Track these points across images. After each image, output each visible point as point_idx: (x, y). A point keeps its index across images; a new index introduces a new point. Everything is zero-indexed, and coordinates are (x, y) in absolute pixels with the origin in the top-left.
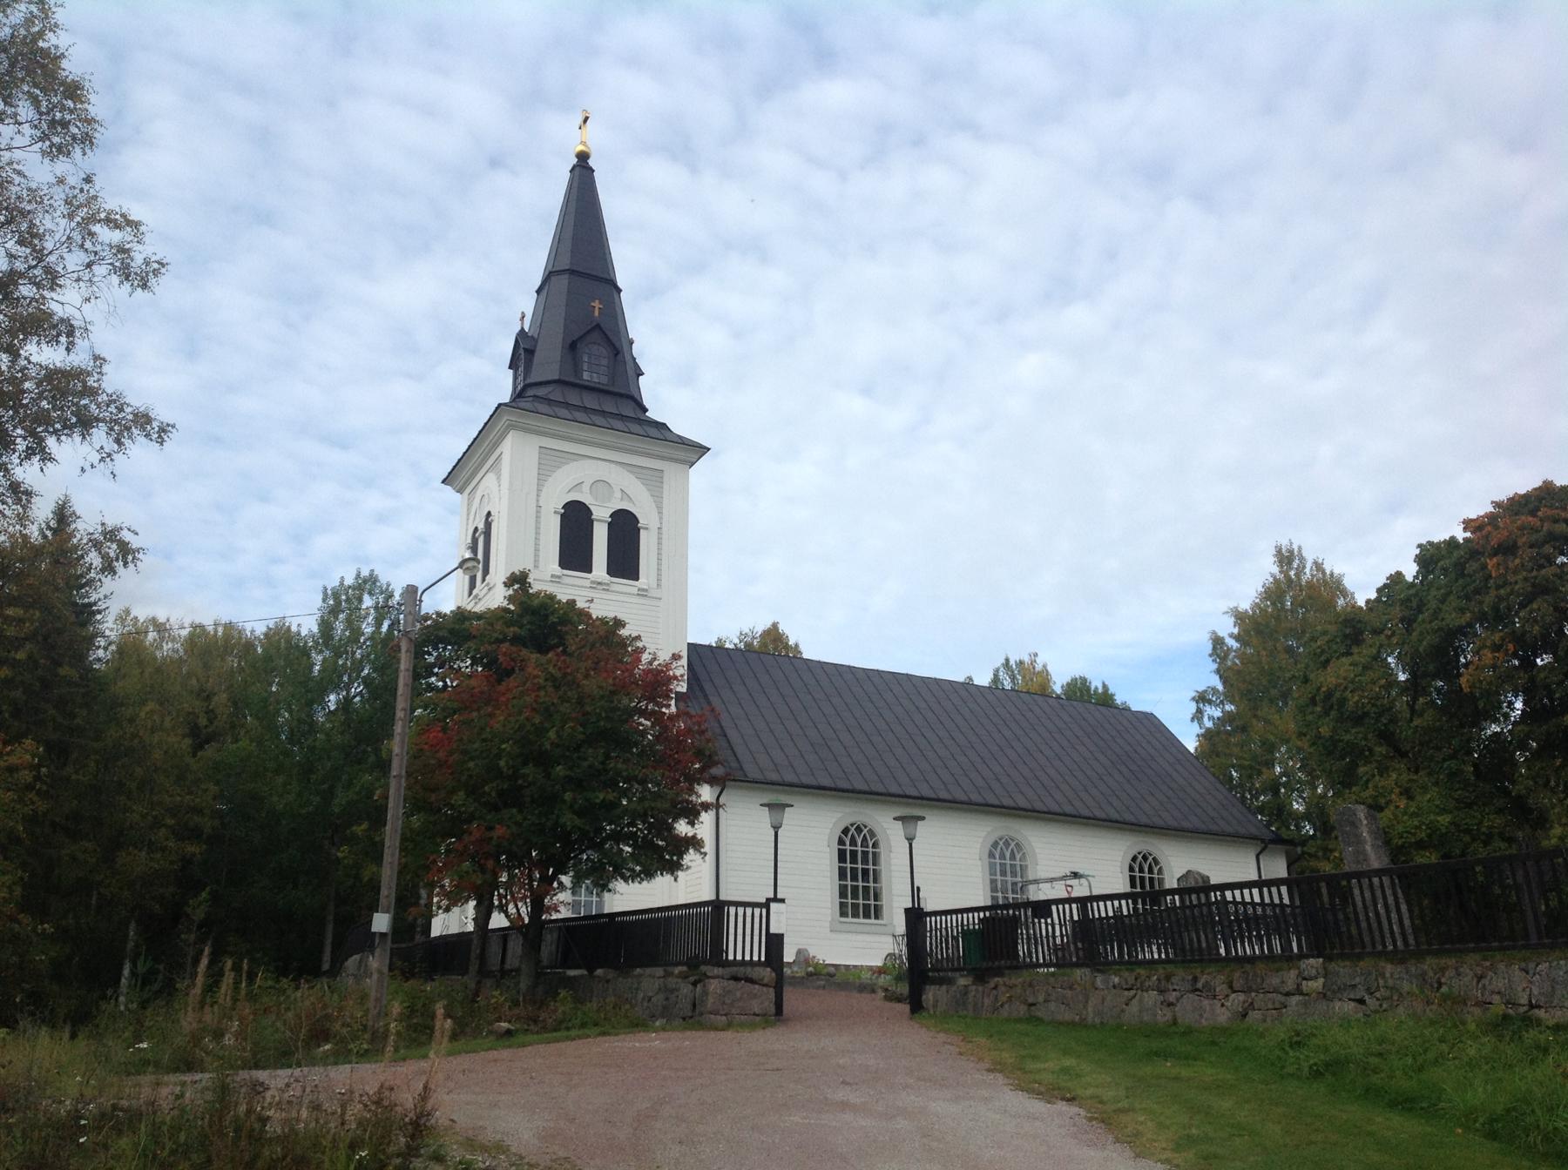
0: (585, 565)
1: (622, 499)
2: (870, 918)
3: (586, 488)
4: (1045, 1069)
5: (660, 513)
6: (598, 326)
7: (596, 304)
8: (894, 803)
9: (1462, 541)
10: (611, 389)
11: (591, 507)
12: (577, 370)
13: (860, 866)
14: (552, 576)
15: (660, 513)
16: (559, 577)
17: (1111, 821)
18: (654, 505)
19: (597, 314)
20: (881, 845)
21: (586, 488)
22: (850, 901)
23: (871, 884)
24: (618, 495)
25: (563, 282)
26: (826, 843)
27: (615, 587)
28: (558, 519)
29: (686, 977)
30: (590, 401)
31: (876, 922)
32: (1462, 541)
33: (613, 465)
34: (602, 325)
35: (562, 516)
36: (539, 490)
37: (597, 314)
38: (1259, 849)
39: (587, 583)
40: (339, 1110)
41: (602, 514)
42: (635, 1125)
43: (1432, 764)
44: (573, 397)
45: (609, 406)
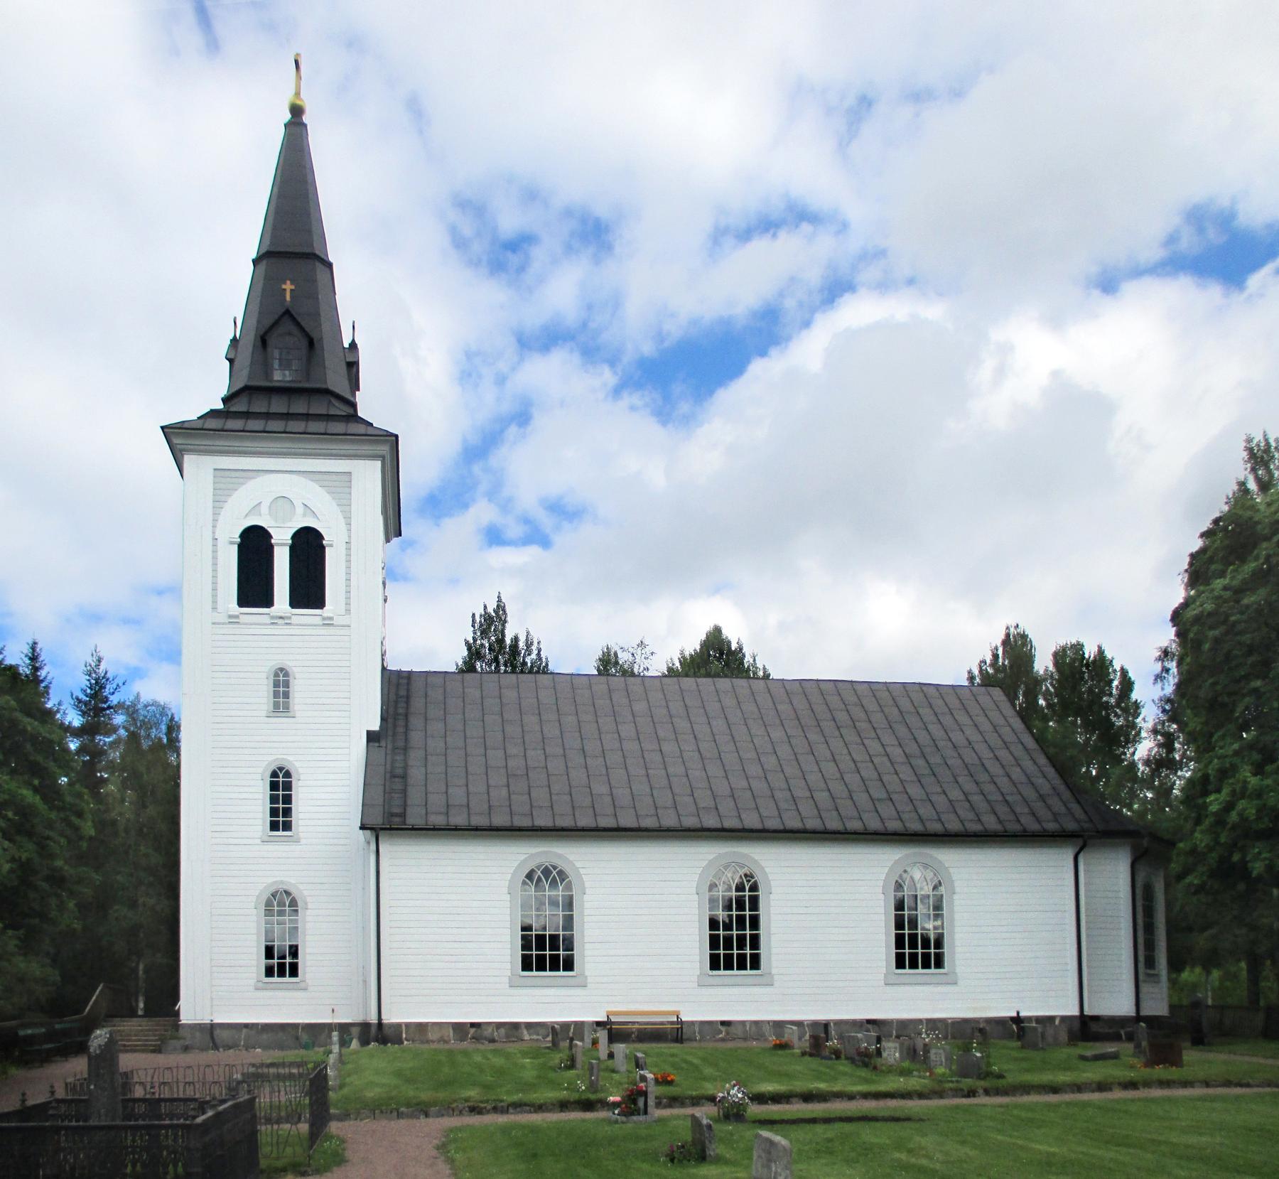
0: (267, 601)
1: (304, 515)
2: (904, 968)
3: (264, 509)
6: (287, 313)
7: (288, 286)
8: (576, 836)
10: (307, 385)
11: (270, 530)
12: (268, 374)
13: (748, 913)
14: (230, 617)
16: (237, 617)
17: (950, 836)
18: (341, 516)
19: (288, 298)
20: (761, 887)
22: (735, 952)
23: (288, 960)
25: (263, 266)
26: (694, 890)
27: (295, 620)
31: (293, 979)
33: (294, 477)
35: (240, 546)
36: (215, 520)
37: (288, 298)
38: (1077, 850)
40: (952, 1159)
41: (282, 538)
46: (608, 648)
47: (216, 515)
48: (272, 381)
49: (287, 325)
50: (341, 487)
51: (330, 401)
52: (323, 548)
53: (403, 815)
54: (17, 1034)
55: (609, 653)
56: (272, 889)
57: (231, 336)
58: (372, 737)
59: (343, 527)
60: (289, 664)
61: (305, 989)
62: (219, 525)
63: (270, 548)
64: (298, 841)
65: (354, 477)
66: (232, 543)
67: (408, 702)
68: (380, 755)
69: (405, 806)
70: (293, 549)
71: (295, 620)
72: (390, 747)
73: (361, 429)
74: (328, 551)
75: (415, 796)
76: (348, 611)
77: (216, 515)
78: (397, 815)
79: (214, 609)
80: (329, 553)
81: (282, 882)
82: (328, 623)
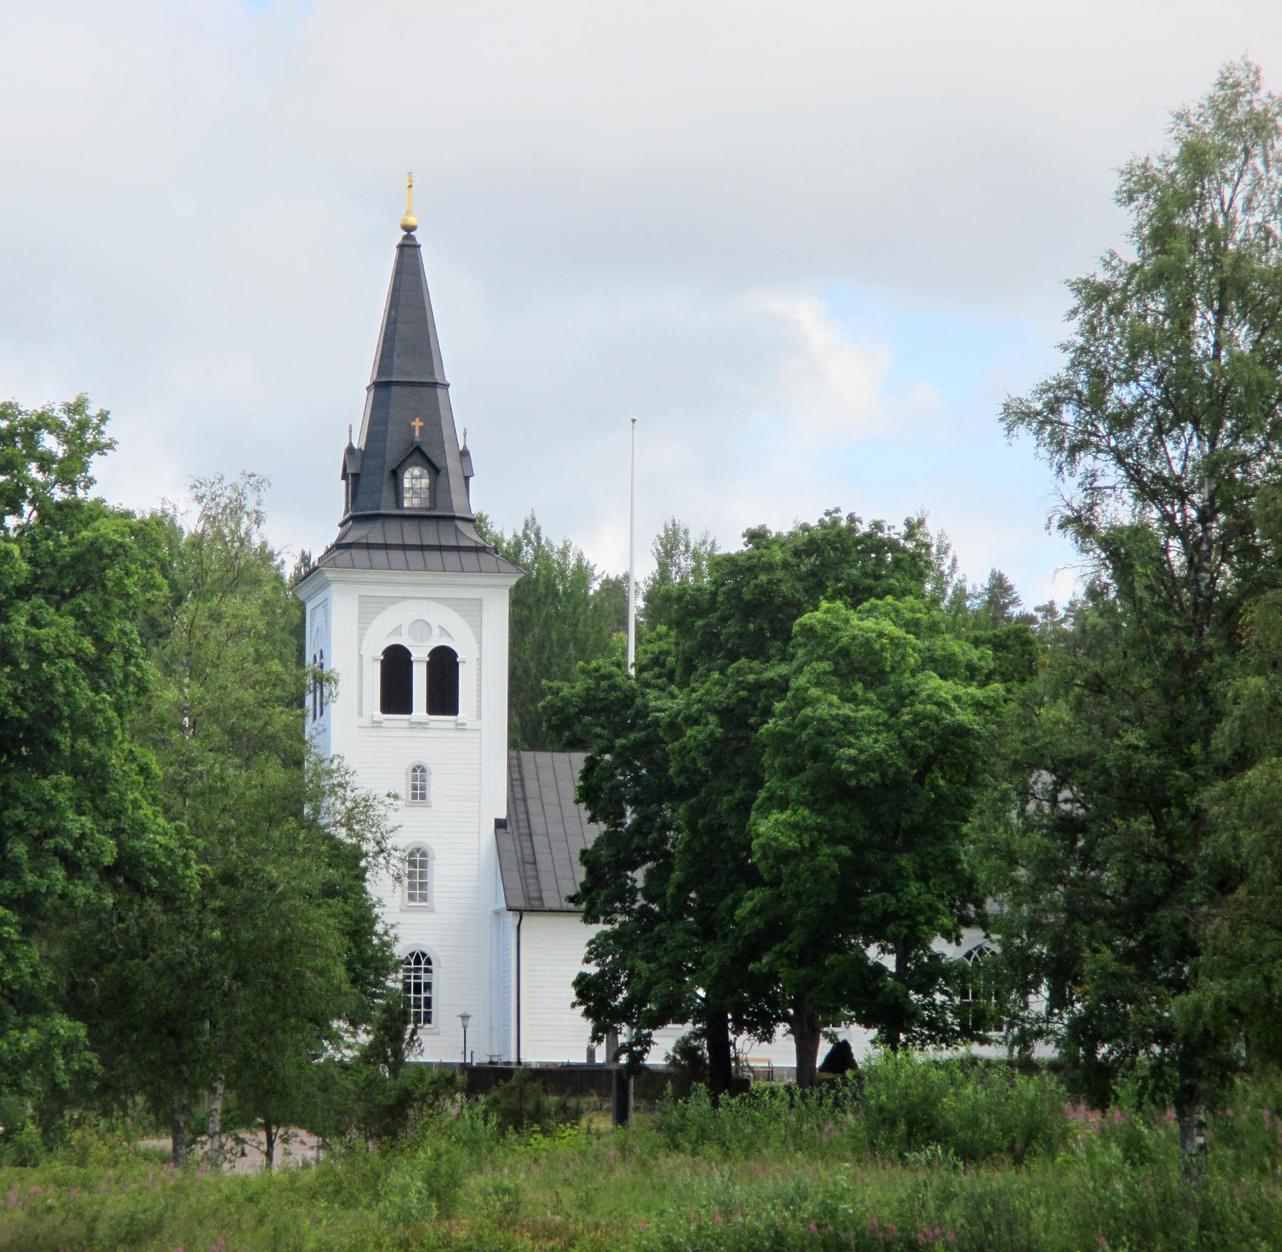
3: (405, 630)
4: (970, 1154)
5: (480, 643)
9: (781, 1029)
15: (480, 643)
19: (417, 434)
21: (405, 630)
23: (423, 1009)
24: (436, 631)
28: (378, 667)
29: (820, 733)
30: (411, 534)
32: (781, 1029)
34: (424, 448)
35: (383, 662)
37: (417, 434)
39: (405, 724)
42: (1226, 671)
43: (174, 996)
44: (393, 534)
45: (430, 535)
46: (674, 525)
47: (360, 640)
48: (403, 508)
49: (417, 453)
50: (471, 613)
51: (457, 529)
52: (457, 664)
53: (540, 899)
54: (599, 1095)
55: (675, 533)
56: (411, 950)
57: (346, 445)
58: (500, 824)
59: (475, 646)
60: (426, 762)
61: (438, 1034)
62: (365, 642)
63: (410, 664)
64: (433, 911)
65: (485, 603)
66: (375, 660)
67: (523, 786)
68: (508, 842)
69: (540, 891)
70: (430, 665)
71: (431, 725)
72: (516, 833)
73: (470, 536)
74: (461, 668)
75: (547, 881)
76: (479, 717)
77: (360, 640)
78: (535, 899)
79: (361, 714)
80: (462, 670)
81: (419, 945)
82: (460, 727)
